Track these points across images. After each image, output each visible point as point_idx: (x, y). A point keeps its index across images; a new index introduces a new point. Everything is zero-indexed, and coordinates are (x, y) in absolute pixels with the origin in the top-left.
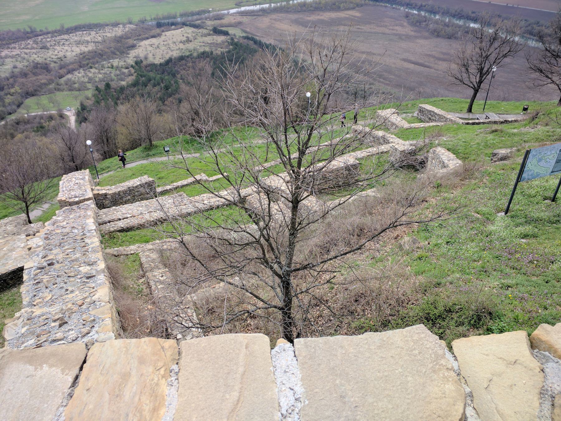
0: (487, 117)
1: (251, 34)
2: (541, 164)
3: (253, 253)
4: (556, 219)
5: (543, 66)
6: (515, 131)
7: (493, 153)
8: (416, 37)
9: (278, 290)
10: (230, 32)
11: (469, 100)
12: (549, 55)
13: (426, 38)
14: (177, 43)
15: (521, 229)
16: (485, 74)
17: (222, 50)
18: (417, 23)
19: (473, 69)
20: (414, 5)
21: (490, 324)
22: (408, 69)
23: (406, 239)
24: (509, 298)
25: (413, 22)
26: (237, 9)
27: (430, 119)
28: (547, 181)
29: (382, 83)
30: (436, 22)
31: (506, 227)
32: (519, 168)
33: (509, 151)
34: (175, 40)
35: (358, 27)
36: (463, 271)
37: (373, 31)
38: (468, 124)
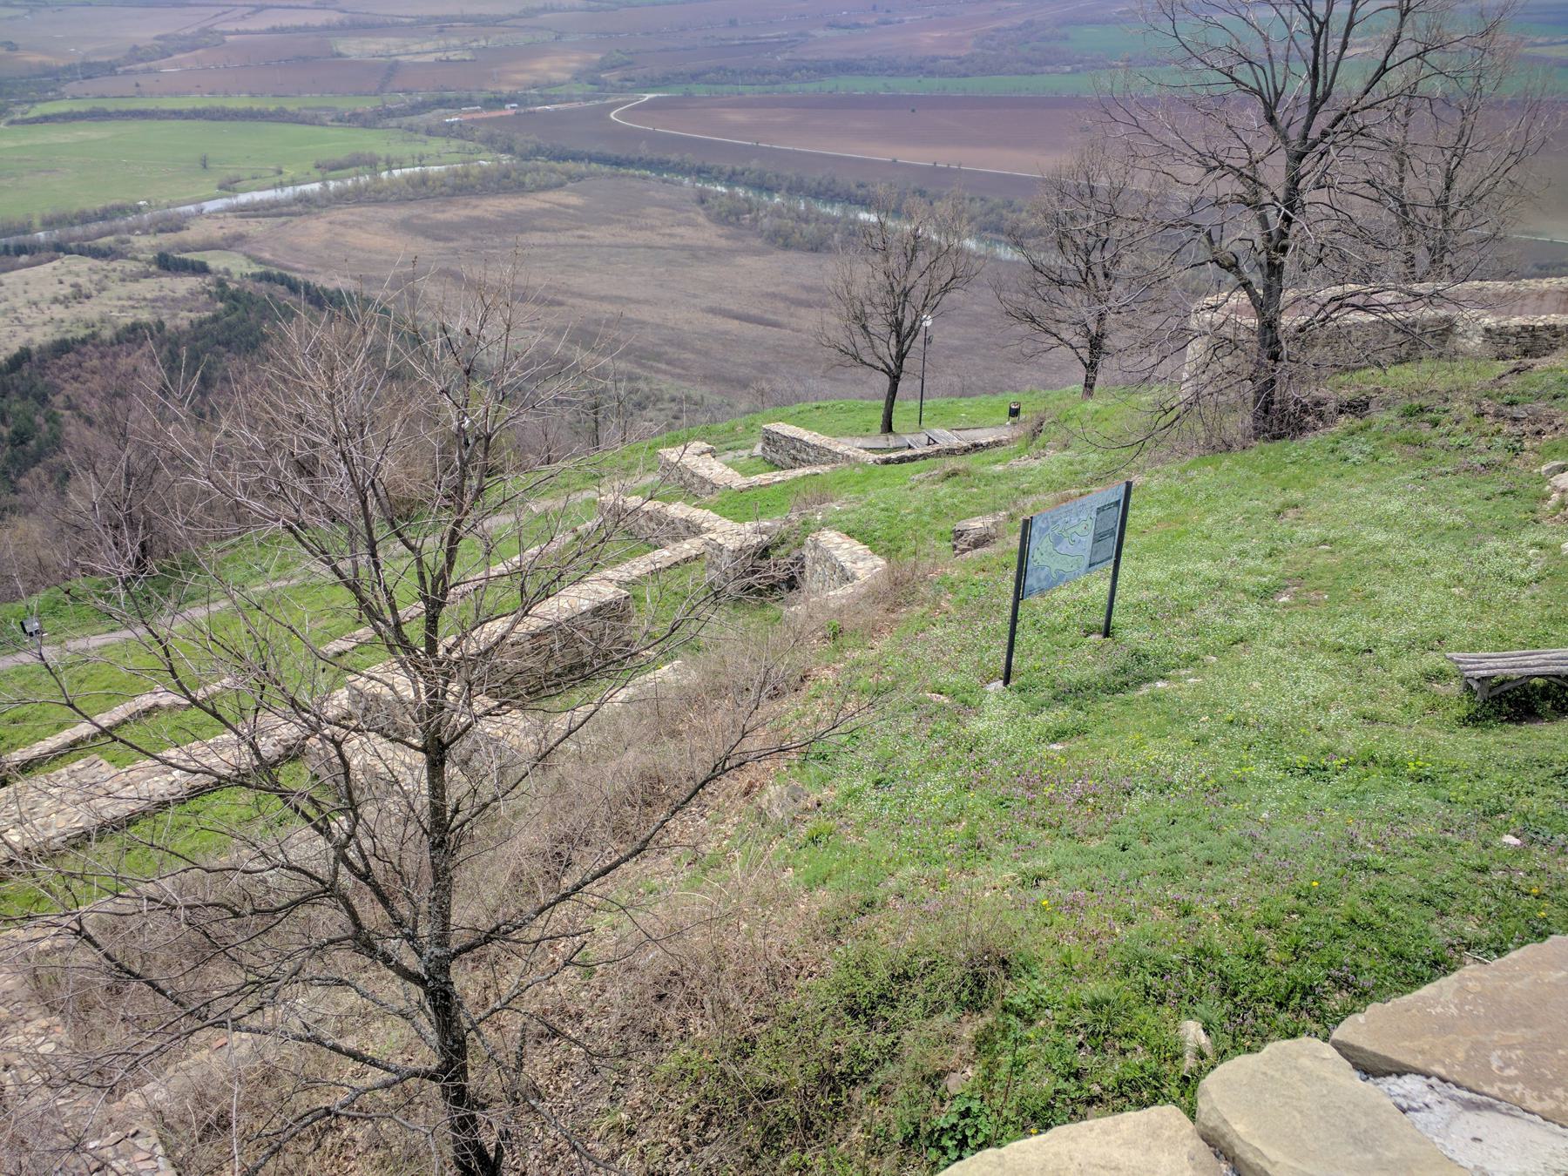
0: (931, 441)
1: (278, 266)
2: (1062, 548)
3: (327, 920)
4: (1120, 679)
5: (1034, 306)
6: (999, 468)
7: (954, 532)
8: (733, 252)
9: (422, 1020)
10: (212, 264)
11: (882, 403)
12: (1043, 279)
13: (758, 252)
14: (43, 306)
15: (1048, 719)
16: (909, 334)
17: (192, 315)
18: (730, 216)
19: (878, 325)
20: (715, 173)
21: (1007, 992)
22: (726, 333)
23: (773, 790)
24: (1043, 909)
25: (719, 214)
26: (226, 201)
27: (795, 459)
28: (1085, 586)
29: (665, 372)
30: (777, 213)
31: (1012, 719)
32: (1016, 557)
33: (990, 520)
34: (34, 296)
35: (580, 232)
36: (924, 858)
37: (619, 241)
38: (887, 462)
